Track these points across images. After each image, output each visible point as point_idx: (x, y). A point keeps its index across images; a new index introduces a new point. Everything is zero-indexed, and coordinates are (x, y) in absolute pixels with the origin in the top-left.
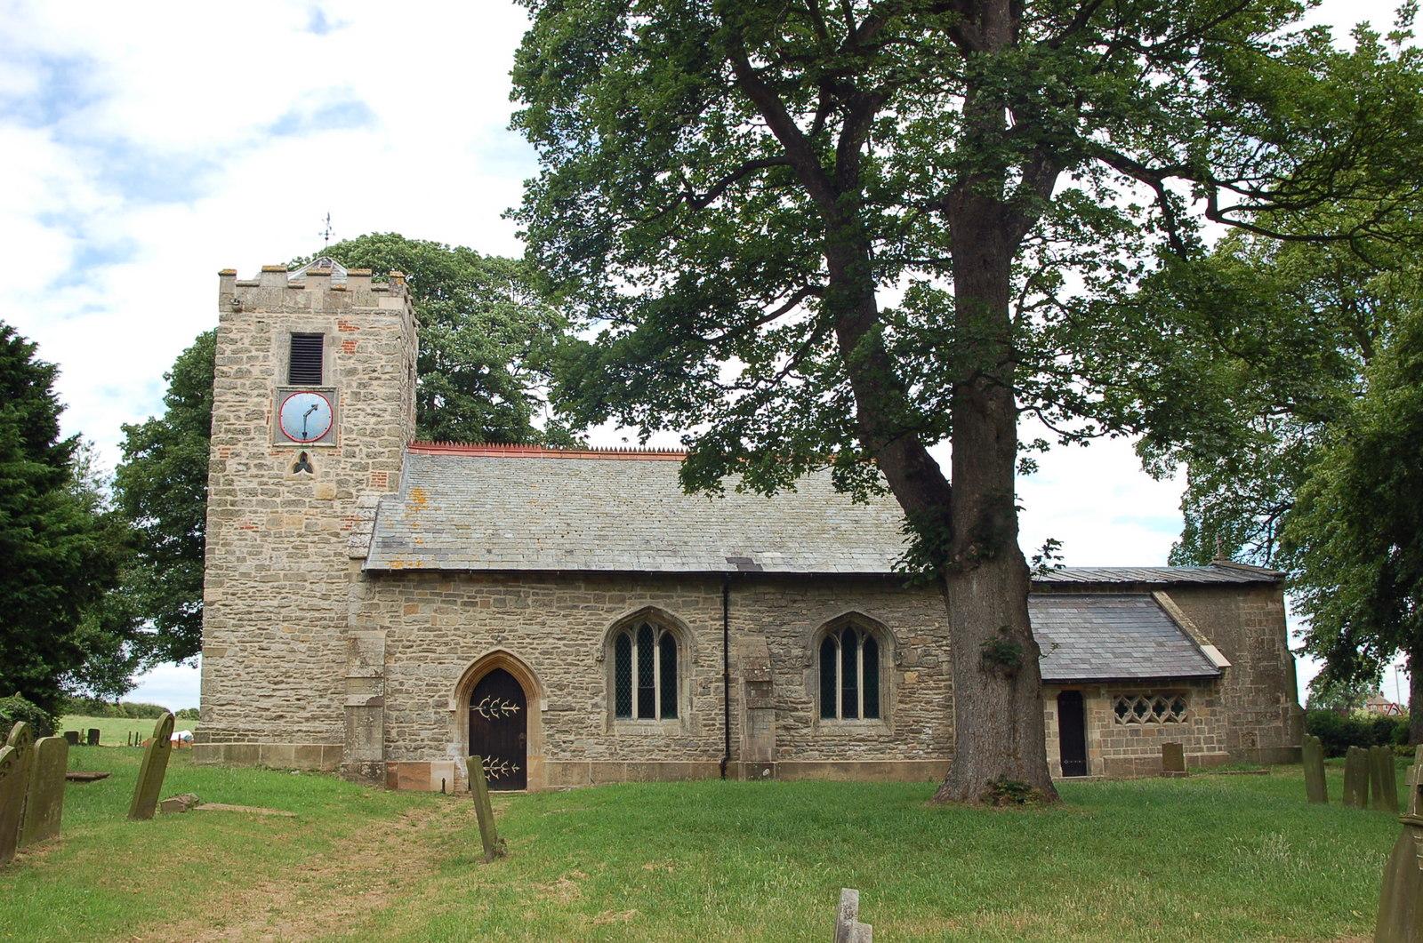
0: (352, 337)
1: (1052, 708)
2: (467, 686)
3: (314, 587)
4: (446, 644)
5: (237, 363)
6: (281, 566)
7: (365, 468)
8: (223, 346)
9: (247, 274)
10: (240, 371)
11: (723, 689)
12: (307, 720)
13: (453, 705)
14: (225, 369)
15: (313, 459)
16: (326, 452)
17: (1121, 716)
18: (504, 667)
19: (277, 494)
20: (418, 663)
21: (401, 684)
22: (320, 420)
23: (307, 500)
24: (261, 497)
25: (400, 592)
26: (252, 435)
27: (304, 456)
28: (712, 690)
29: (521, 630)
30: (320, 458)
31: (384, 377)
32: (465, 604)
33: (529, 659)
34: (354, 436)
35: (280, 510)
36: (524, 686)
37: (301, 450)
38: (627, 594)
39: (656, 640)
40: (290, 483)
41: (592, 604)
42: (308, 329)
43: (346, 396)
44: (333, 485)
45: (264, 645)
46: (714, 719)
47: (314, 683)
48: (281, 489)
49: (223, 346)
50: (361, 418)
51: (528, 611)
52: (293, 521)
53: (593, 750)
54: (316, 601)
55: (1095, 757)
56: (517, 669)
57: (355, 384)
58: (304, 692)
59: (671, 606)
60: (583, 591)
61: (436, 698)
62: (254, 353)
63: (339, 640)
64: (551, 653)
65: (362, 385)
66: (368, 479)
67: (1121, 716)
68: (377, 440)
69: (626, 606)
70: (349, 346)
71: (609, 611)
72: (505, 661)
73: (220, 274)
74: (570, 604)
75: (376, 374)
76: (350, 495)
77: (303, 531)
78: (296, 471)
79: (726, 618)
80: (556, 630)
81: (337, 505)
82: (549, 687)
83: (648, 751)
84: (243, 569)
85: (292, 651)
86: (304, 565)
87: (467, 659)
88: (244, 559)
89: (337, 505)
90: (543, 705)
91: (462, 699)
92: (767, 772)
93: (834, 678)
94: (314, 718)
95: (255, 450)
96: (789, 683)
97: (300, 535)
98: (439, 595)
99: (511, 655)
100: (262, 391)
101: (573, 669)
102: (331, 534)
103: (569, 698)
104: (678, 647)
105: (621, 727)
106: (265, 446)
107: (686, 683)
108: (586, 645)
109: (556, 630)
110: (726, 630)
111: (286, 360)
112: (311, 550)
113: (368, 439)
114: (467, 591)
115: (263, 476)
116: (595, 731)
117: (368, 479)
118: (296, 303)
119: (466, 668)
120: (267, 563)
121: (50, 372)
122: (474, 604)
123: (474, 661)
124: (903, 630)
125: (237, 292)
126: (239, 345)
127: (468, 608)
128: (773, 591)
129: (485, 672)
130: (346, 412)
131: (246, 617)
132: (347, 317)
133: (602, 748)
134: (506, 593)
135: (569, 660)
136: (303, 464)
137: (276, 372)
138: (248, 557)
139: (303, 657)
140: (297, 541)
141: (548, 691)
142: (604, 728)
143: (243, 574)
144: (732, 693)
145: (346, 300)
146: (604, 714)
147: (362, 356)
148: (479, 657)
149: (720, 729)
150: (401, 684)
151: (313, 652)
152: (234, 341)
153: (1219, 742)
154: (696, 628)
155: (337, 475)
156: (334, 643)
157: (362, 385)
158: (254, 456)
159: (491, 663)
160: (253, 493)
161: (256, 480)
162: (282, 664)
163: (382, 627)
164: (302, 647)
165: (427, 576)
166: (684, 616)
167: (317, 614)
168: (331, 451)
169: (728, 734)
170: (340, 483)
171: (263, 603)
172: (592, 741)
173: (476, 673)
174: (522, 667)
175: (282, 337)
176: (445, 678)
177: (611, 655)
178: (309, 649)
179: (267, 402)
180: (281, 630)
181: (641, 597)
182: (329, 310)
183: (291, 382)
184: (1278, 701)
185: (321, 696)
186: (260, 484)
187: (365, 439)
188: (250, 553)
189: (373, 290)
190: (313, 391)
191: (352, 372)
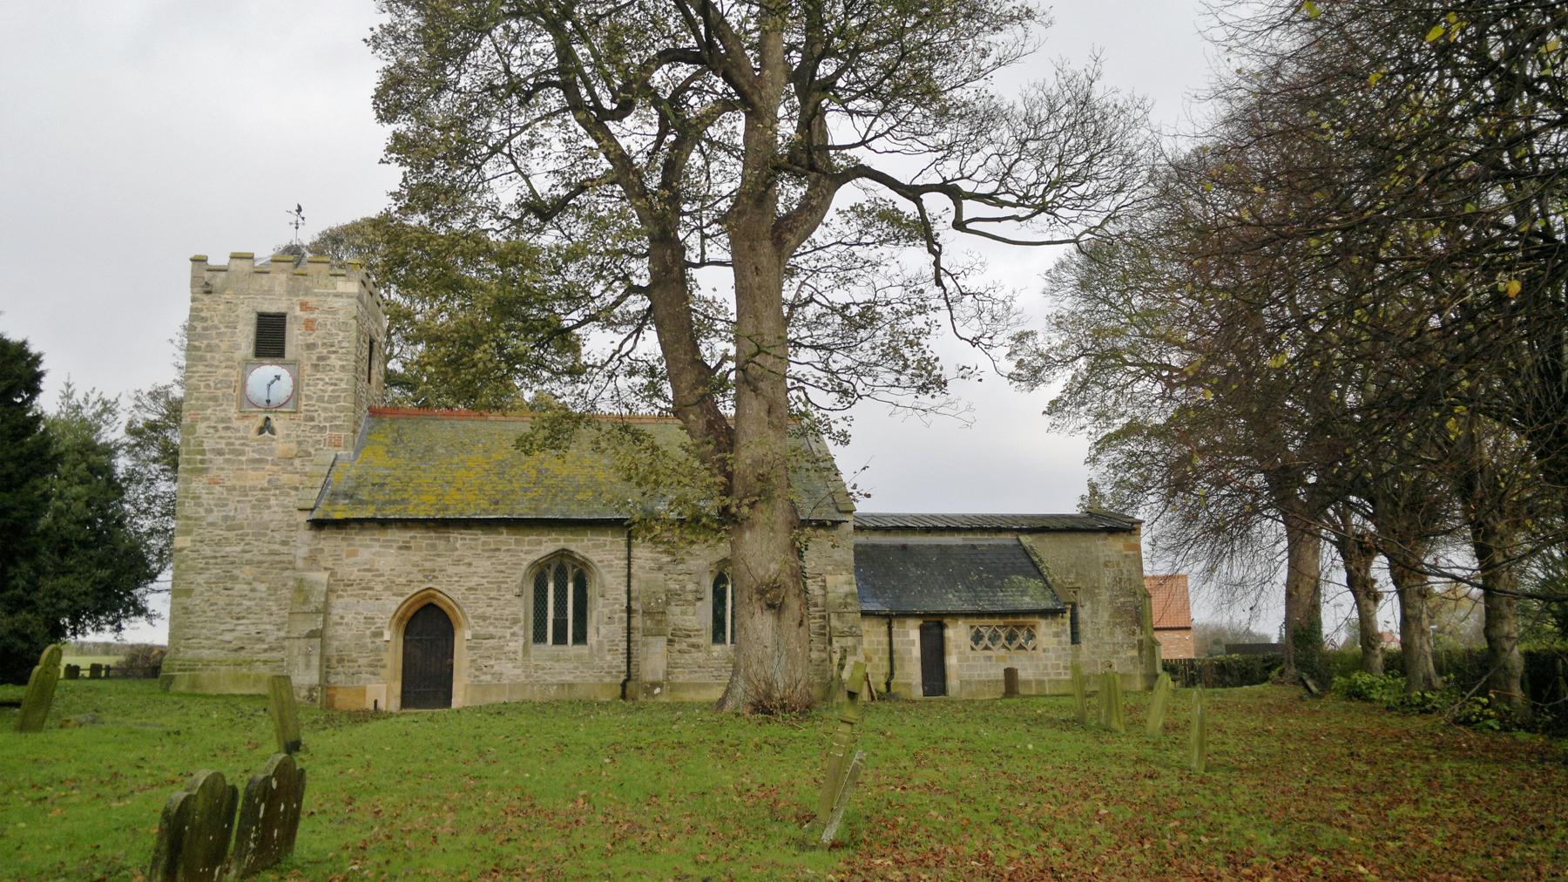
1: (915, 635)
2: (401, 619)
9: (218, 258)
10: (209, 345)
12: (265, 651)
15: (275, 423)
16: (287, 416)
17: (977, 644)
18: (435, 602)
19: (242, 453)
21: (342, 618)
32: (400, 548)
33: (456, 594)
34: (313, 402)
36: (451, 617)
38: (544, 539)
39: (570, 577)
41: (513, 547)
42: (272, 308)
44: (293, 445)
45: (229, 585)
47: (273, 618)
50: (320, 387)
51: (456, 553)
52: (257, 478)
53: (510, 671)
54: (276, 547)
55: (953, 683)
56: (446, 603)
57: (314, 357)
58: (262, 627)
59: (582, 545)
62: (223, 330)
65: (321, 358)
67: (977, 644)
68: (333, 406)
70: (309, 325)
71: (527, 553)
72: (433, 596)
73: (192, 260)
74: (492, 547)
76: (309, 454)
79: (629, 558)
81: (297, 462)
82: (473, 618)
84: (210, 519)
85: (253, 590)
86: (266, 515)
87: (402, 595)
88: (211, 511)
89: (297, 462)
90: (468, 634)
92: (657, 690)
93: (556, 609)
94: (271, 649)
95: (223, 415)
96: (683, 613)
98: (378, 540)
100: (229, 363)
101: (494, 602)
102: (291, 488)
105: (536, 649)
106: (233, 412)
107: (595, 614)
109: (481, 570)
110: (629, 568)
111: (252, 337)
112: (273, 502)
113: (326, 405)
114: (428, 528)
116: (513, 656)
120: (232, 514)
121: (24, 343)
122: (408, 548)
123: (407, 597)
125: (207, 275)
126: (209, 323)
129: (417, 607)
131: (212, 561)
133: (518, 671)
134: (439, 538)
135: (492, 594)
136: (267, 427)
138: (215, 509)
139: (263, 595)
140: (260, 495)
142: (520, 654)
143: (211, 524)
146: (521, 641)
148: (411, 593)
150: (342, 618)
153: (1065, 668)
154: (604, 567)
158: (222, 420)
159: (423, 598)
160: (220, 453)
161: (223, 441)
163: (326, 569)
164: (263, 587)
165: (367, 525)
166: (594, 556)
167: (277, 558)
169: (629, 658)
170: (299, 443)
171: (228, 549)
172: (510, 665)
173: (409, 607)
175: (249, 316)
176: (381, 612)
177: (530, 590)
179: (234, 373)
180: (246, 572)
181: (558, 540)
184: (1134, 633)
185: (279, 630)
186: (227, 444)
188: (216, 505)
191: (311, 347)
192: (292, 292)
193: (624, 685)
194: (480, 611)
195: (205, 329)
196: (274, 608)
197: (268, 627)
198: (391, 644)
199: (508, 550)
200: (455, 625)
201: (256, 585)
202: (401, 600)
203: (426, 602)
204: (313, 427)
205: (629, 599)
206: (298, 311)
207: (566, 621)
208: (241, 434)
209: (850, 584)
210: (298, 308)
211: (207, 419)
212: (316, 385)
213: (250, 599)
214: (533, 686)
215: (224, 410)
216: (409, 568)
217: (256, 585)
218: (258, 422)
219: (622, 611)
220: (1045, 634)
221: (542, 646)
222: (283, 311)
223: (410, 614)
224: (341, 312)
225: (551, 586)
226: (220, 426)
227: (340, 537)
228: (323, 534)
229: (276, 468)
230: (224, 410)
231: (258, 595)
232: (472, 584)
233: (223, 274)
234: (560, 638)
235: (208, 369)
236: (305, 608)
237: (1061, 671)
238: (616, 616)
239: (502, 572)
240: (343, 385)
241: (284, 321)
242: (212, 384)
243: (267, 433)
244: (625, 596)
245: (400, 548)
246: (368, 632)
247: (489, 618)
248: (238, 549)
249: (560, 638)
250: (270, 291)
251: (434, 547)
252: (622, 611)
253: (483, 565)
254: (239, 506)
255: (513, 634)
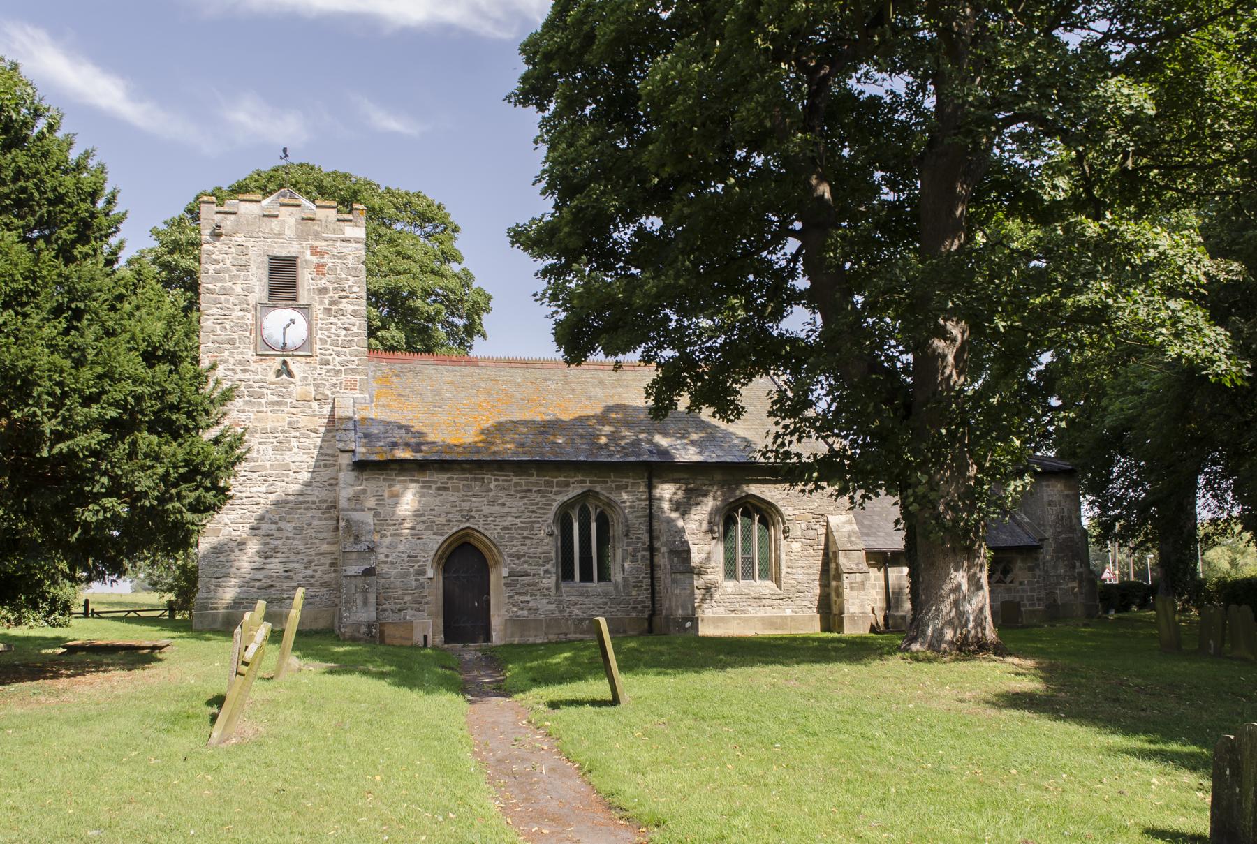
0: (322, 261)
2: (441, 558)
3: (296, 474)
4: (424, 522)
5: (221, 281)
6: (267, 457)
7: (338, 372)
8: (207, 266)
10: (223, 288)
11: (648, 557)
13: (430, 573)
14: (210, 286)
15: (293, 367)
16: (304, 359)
18: (472, 541)
20: (823, 543)
21: (387, 556)
22: (297, 334)
23: (289, 401)
24: (247, 398)
25: (384, 480)
26: (237, 344)
27: (285, 363)
28: (640, 557)
29: (486, 510)
30: (298, 364)
31: (351, 295)
32: (439, 489)
35: (265, 409)
36: (488, 556)
37: (282, 358)
38: (571, 480)
39: (593, 517)
40: (273, 386)
42: (284, 253)
43: (318, 311)
46: (641, 582)
47: (299, 557)
48: (266, 391)
49: (207, 266)
50: (333, 331)
51: (491, 494)
53: (545, 606)
56: (482, 542)
57: (326, 301)
58: (291, 565)
60: (535, 478)
61: (416, 567)
62: (235, 273)
63: (320, 519)
64: (510, 529)
66: (341, 383)
69: (570, 489)
70: (320, 269)
71: (557, 493)
72: (471, 536)
74: (524, 488)
75: (344, 293)
77: (286, 427)
78: (278, 376)
80: (514, 510)
81: (315, 404)
83: (590, 608)
87: (441, 535)
90: (505, 572)
91: (437, 569)
93: (760, 548)
97: (283, 431)
98: (417, 481)
99: (478, 531)
101: (528, 542)
103: (526, 566)
104: (611, 523)
106: (250, 354)
108: (538, 522)
109: (514, 510)
111: (265, 280)
112: (294, 443)
113: (340, 349)
114: (464, 471)
115: (249, 380)
117: (341, 383)
118: (272, 230)
119: (440, 542)
122: (446, 489)
123: (446, 536)
124: (790, 508)
127: (441, 492)
128: (686, 476)
129: (455, 545)
130: (320, 325)
132: (317, 243)
133: (552, 607)
134: (475, 479)
135: (526, 533)
137: (257, 289)
139: (290, 535)
141: (508, 560)
142: (553, 590)
144: (656, 559)
145: (316, 228)
146: (554, 578)
147: (331, 277)
148: (451, 532)
149: (646, 590)
151: (299, 530)
152: (216, 262)
153: (1039, 599)
155: (314, 380)
156: (316, 523)
157: (332, 303)
158: (240, 363)
162: (272, 541)
164: (288, 527)
165: (406, 466)
168: (309, 359)
170: (317, 386)
171: (253, 490)
172: (545, 601)
173: (449, 546)
174: (487, 540)
175: (260, 259)
176: (423, 551)
178: (295, 528)
179: (249, 316)
181: (583, 482)
182: (301, 236)
183: (270, 300)
184: (1074, 567)
185: (306, 568)
187: (335, 349)
189: (339, 220)
190: (286, 307)
191: (322, 291)
192: (301, 236)
193: (650, 619)
194: (514, 549)
195: (218, 272)
196: (301, 547)
197: (296, 565)
198: (434, 584)
199: (538, 491)
200: (491, 562)
201: (281, 524)
202: (442, 539)
203: (462, 540)
204: (328, 371)
205: (652, 538)
206: (308, 255)
207: (591, 558)
208: (259, 377)
209: (851, 523)
210: (308, 252)
211: (226, 361)
212: (329, 329)
213: (277, 539)
214: (567, 620)
215: (242, 353)
216: (447, 508)
217: (281, 524)
218: (277, 363)
219: (644, 550)
220: (1021, 569)
221: (571, 584)
222: (294, 255)
223: (448, 553)
224: (350, 257)
225: (576, 526)
226: (238, 369)
227: (382, 478)
228: (365, 475)
229: (294, 411)
230: (242, 353)
231: (286, 534)
232: (505, 524)
233: (233, 217)
234: (586, 576)
235: (223, 312)
236: (358, 547)
237: (1036, 602)
238: (639, 555)
239: (533, 512)
240: (355, 330)
241: (295, 265)
242: (228, 327)
243: (284, 376)
244: (647, 535)
245: (439, 489)
246: (411, 570)
247: (523, 556)
248: (263, 489)
249: (586, 576)
250: (280, 235)
251: (469, 487)
252: (644, 550)
253: (516, 505)
254: (261, 447)
255: (546, 572)
